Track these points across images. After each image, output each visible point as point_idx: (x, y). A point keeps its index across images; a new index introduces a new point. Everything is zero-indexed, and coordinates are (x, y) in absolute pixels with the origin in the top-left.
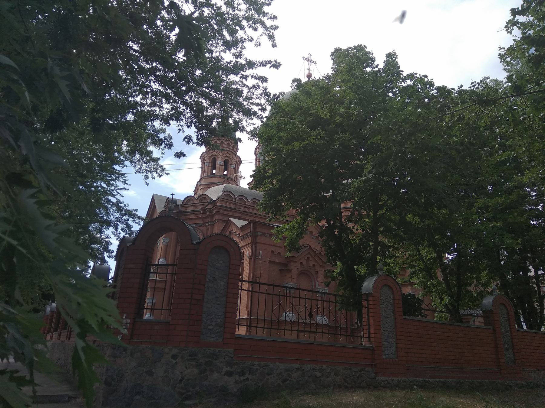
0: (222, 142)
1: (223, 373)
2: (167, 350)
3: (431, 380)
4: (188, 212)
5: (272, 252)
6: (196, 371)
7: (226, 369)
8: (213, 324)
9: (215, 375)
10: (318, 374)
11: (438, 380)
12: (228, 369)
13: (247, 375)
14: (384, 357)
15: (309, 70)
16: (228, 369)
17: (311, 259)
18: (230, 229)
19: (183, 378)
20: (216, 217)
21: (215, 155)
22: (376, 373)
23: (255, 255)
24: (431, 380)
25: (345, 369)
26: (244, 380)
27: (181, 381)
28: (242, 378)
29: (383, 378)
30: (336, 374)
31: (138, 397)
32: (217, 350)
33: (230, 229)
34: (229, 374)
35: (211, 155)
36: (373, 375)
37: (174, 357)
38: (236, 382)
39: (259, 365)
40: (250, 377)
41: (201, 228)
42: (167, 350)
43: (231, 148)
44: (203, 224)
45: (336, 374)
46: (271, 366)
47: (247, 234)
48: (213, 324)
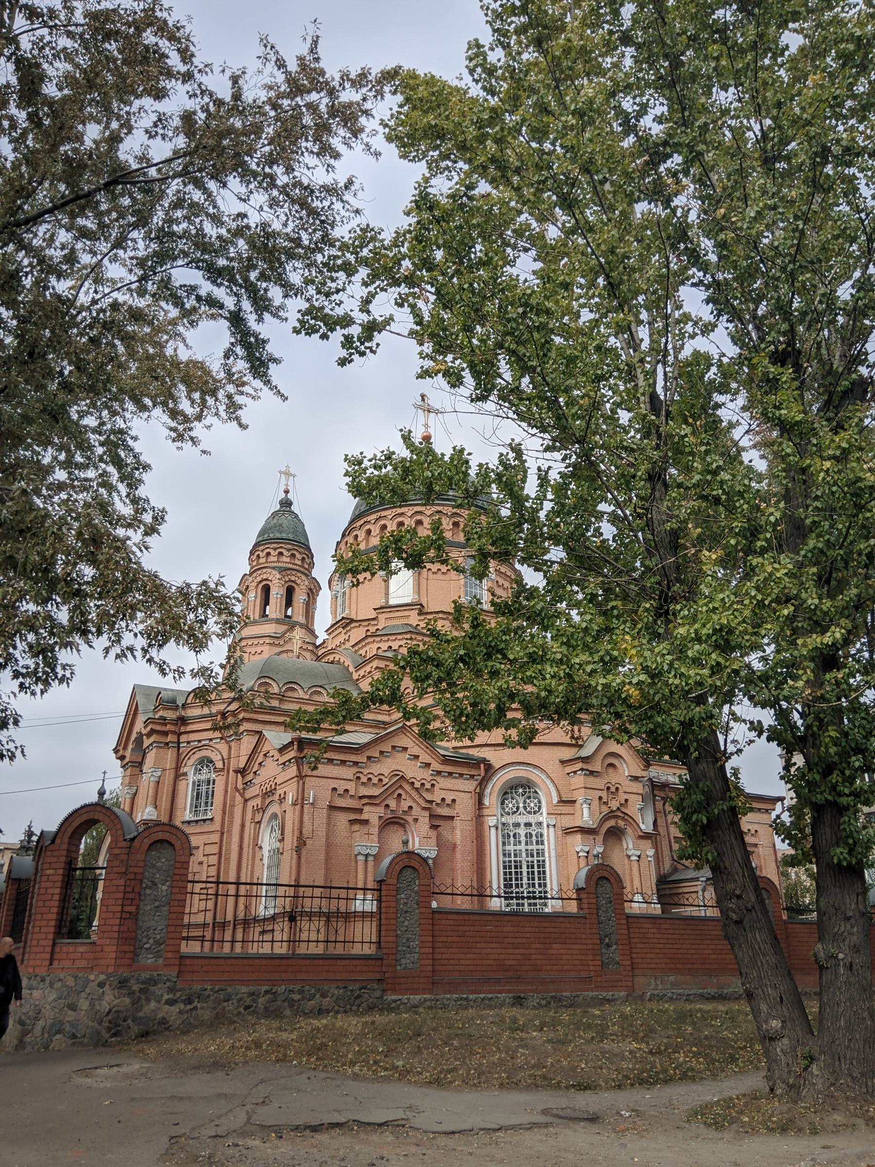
0: (281, 554)
1: (163, 1001)
2: (92, 977)
3: (471, 997)
4: (195, 718)
5: (334, 789)
6: (127, 1000)
7: (166, 997)
8: (151, 941)
9: (153, 1005)
10: (296, 997)
11: (482, 996)
12: (171, 996)
13: (195, 1003)
14: (398, 968)
15: (426, 426)
16: (171, 996)
17: (404, 797)
18: (265, 749)
19: (110, 1010)
20: (242, 729)
21: (266, 580)
22: (383, 991)
23: (303, 799)
24: (471, 997)
25: (337, 987)
26: (191, 1010)
27: (108, 1013)
28: (189, 1007)
29: (394, 997)
30: (324, 996)
31: (58, 1036)
32: (155, 974)
33: (265, 749)
34: (171, 1002)
35: (259, 579)
36: (378, 993)
37: (101, 985)
38: (181, 1012)
39: (212, 990)
40: (199, 1005)
41: (217, 746)
42: (92, 977)
43: (299, 563)
44: (222, 738)
45: (324, 996)
46: (229, 990)
47: (289, 761)
48: (151, 941)
